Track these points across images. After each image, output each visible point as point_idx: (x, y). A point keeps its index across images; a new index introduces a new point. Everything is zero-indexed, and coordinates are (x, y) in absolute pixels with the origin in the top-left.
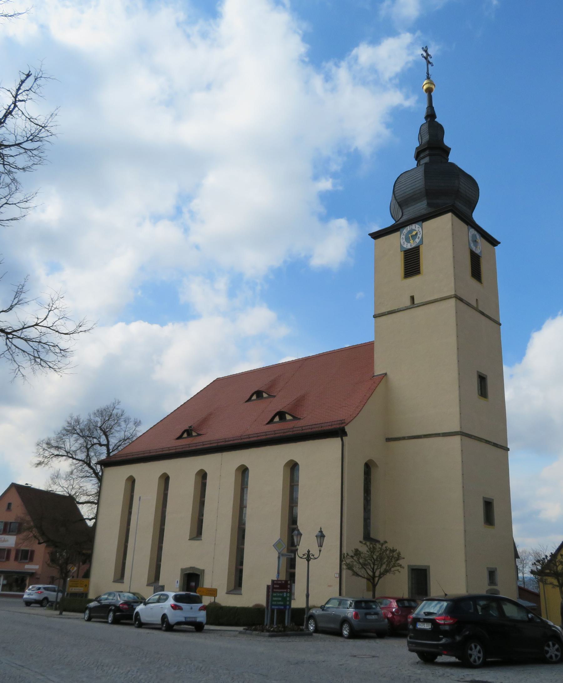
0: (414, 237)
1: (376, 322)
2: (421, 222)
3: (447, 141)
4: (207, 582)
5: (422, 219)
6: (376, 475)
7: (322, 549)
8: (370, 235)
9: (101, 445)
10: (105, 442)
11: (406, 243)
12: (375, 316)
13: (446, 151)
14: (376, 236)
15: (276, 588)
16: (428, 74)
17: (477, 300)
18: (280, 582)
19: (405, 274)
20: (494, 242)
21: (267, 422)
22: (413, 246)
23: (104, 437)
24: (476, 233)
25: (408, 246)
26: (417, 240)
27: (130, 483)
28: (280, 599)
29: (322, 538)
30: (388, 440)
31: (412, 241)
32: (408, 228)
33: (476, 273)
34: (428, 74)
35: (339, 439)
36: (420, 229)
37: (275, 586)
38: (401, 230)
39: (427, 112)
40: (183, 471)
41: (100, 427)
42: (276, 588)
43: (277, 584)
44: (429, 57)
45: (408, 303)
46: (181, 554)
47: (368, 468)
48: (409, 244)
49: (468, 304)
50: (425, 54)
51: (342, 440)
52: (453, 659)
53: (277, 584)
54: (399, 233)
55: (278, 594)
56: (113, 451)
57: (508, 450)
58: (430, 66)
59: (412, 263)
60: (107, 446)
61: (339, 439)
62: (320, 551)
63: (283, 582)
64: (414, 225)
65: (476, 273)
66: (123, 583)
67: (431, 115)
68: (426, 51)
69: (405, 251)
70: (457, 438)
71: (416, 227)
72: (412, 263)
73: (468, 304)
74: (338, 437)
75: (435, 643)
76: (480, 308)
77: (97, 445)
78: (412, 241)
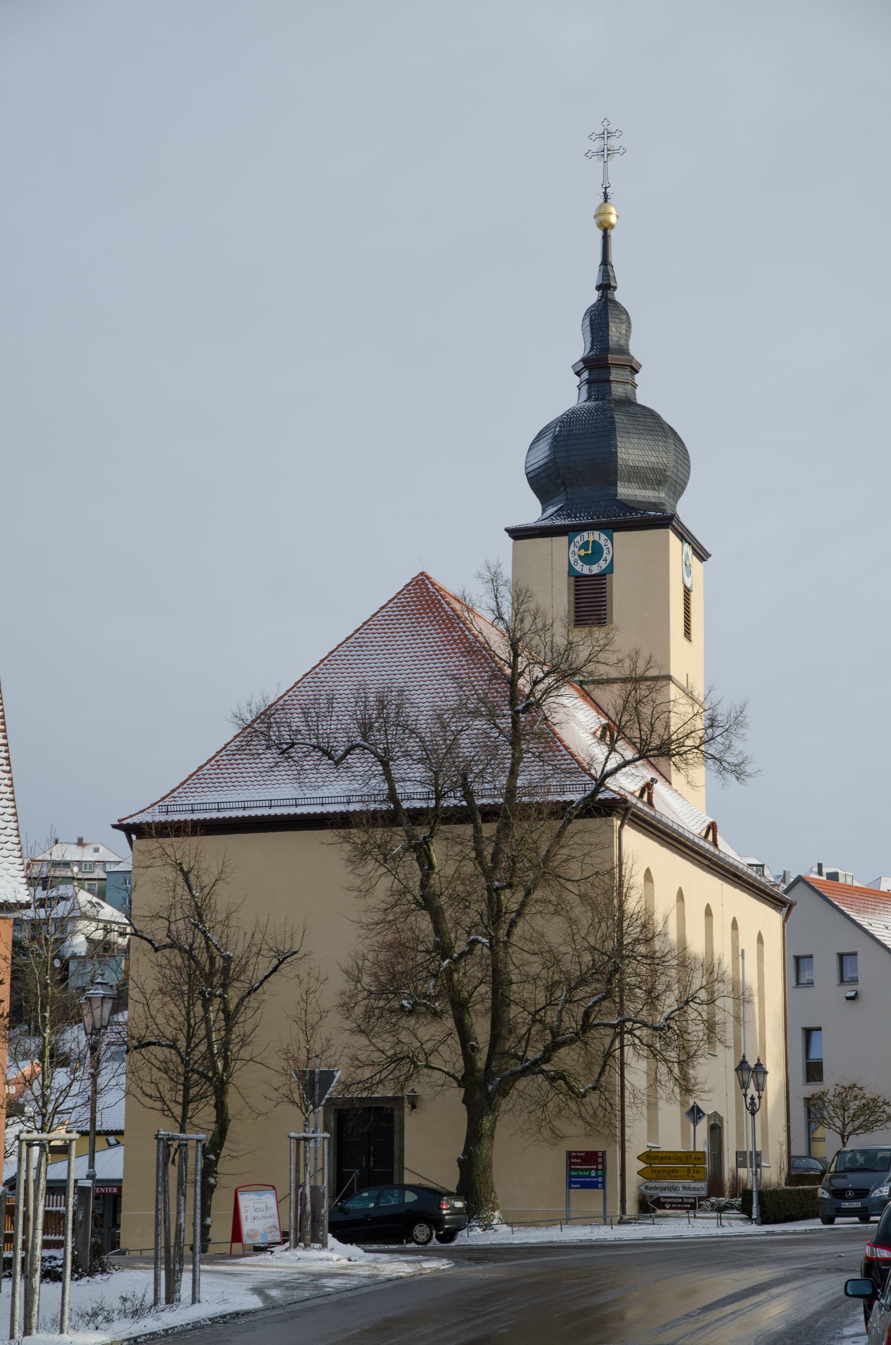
8: (507, 530)
15: (575, 1164)
36: (609, 543)
42: (575, 1164)
43: (577, 1157)
67: (606, 286)
69: (576, 577)
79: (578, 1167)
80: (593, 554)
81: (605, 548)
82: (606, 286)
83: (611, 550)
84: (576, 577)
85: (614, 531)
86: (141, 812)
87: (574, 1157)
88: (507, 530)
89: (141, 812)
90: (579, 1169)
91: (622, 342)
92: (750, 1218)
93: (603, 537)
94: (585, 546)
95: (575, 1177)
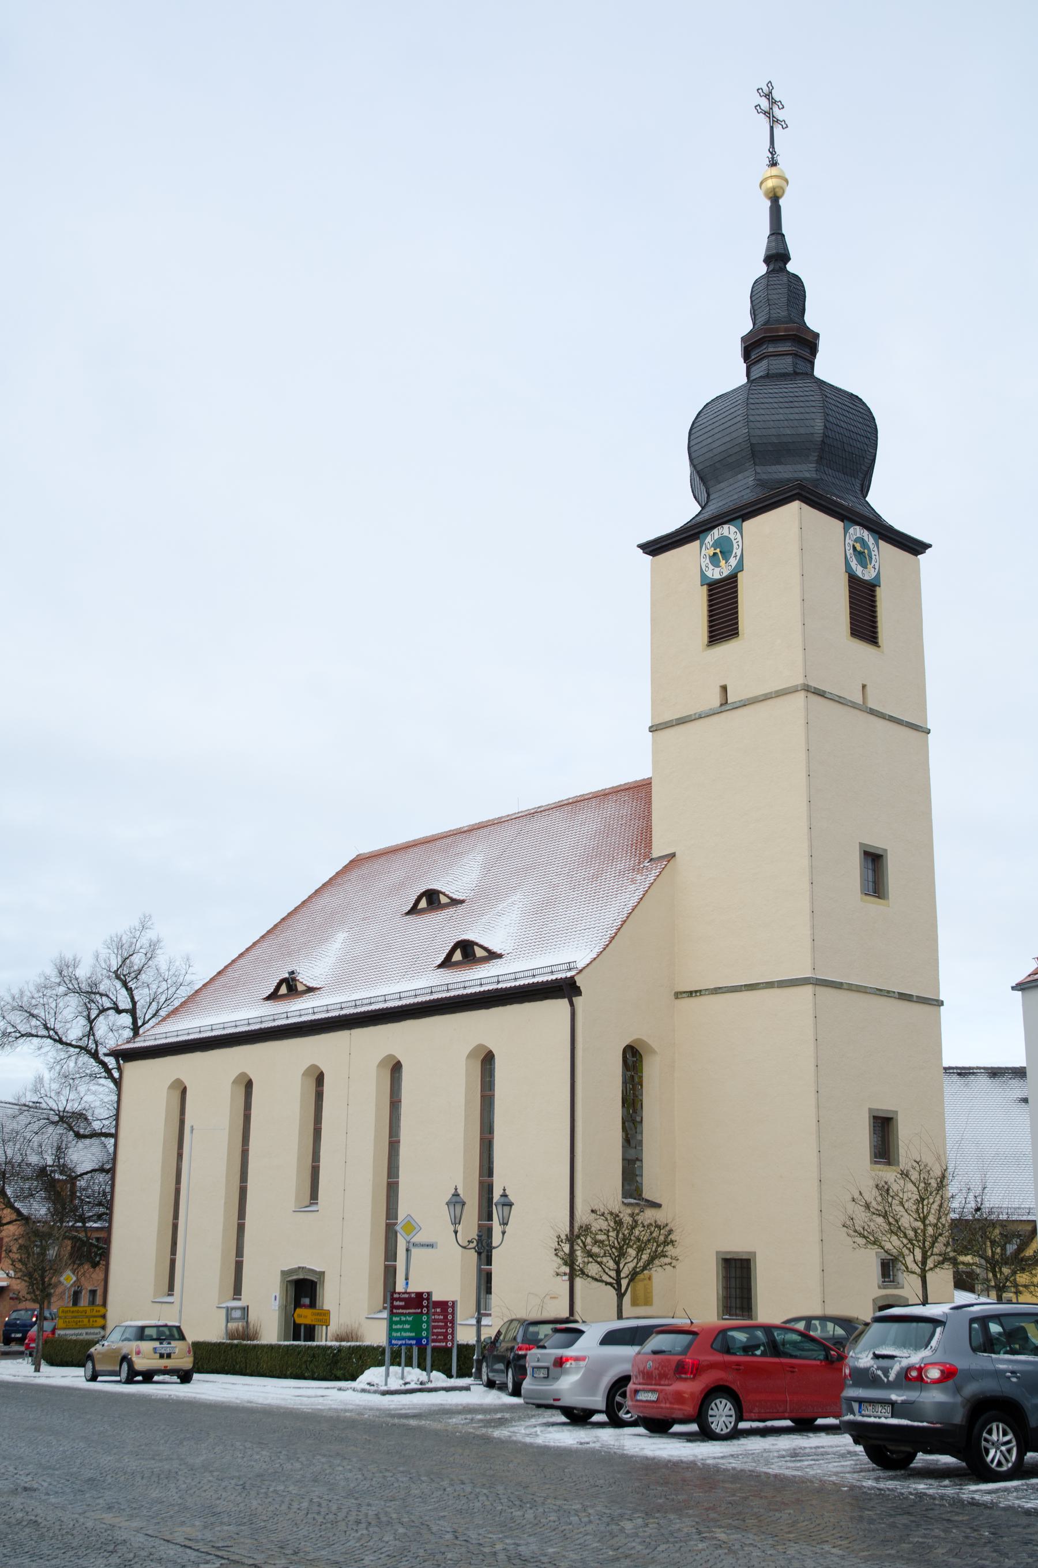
0: (726, 554)
1: (654, 742)
2: (740, 520)
3: (812, 320)
4: (329, 1297)
5: (741, 514)
6: (652, 1072)
7: (508, 1228)
8: (640, 546)
9: (119, 1011)
10: (128, 1005)
11: (711, 567)
12: (653, 729)
13: (807, 344)
14: (655, 548)
15: (398, 1307)
16: (773, 152)
17: (864, 686)
18: (406, 1296)
19: (710, 637)
20: (915, 547)
21: (439, 962)
22: (726, 573)
23: (124, 992)
24: (866, 535)
25: (715, 574)
26: (733, 562)
27: (177, 1094)
28: (407, 1326)
29: (506, 1208)
30: (678, 995)
31: (723, 563)
32: (716, 533)
33: (864, 623)
34: (773, 152)
35: (566, 1001)
36: (739, 535)
37: (396, 1303)
38: (701, 536)
39: (768, 249)
40: (280, 1067)
41: (116, 972)
42: (398, 1307)
43: (400, 1299)
44: (775, 109)
45: (715, 701)
46: (281, 1244)
47: (633, 1058)
48: (717, 570)
49: (840, 701)
50: (765, 104)
51: (572, 1004)
52: (947, 1460)
53: (400, 1299)
54: (698, 542)
55: (403, 1319)
56: (144, 1024)
57: (941, 1003)
58: (778, 130)
59: (723, 616)
60: (133, 1012)
61: (566, 1001)
62: (504, 1233)
63: (413, 1295)
64: (726, 527)
65: (864, 623)
66: (453, 1303)
67: (777, 257)
68: (768, 96)
69: (709, 585)
70: (808, 990)
71: (728, 530)
72: (723, 616)
73: (840, 701)
74: (563, 997)
75: (916, 1424)
76: (871, 704)
77: (111, 1012)
78: (723, 563)
79: (400, 1311)
80: (724, 549)
81: (734, 542)
82: (777, 257)
83: (740, 543)
84: (709, 585)
85: (743, 521)
86: (180, 1312)
87: (397, 1299)
88: (640, 546)
89: (180, 1312)
90: (402, 1314)
91: (782, 251)
92: (450, 1376)
93: (733, 529)
94: (716, 544)
95: (397, 1330)
